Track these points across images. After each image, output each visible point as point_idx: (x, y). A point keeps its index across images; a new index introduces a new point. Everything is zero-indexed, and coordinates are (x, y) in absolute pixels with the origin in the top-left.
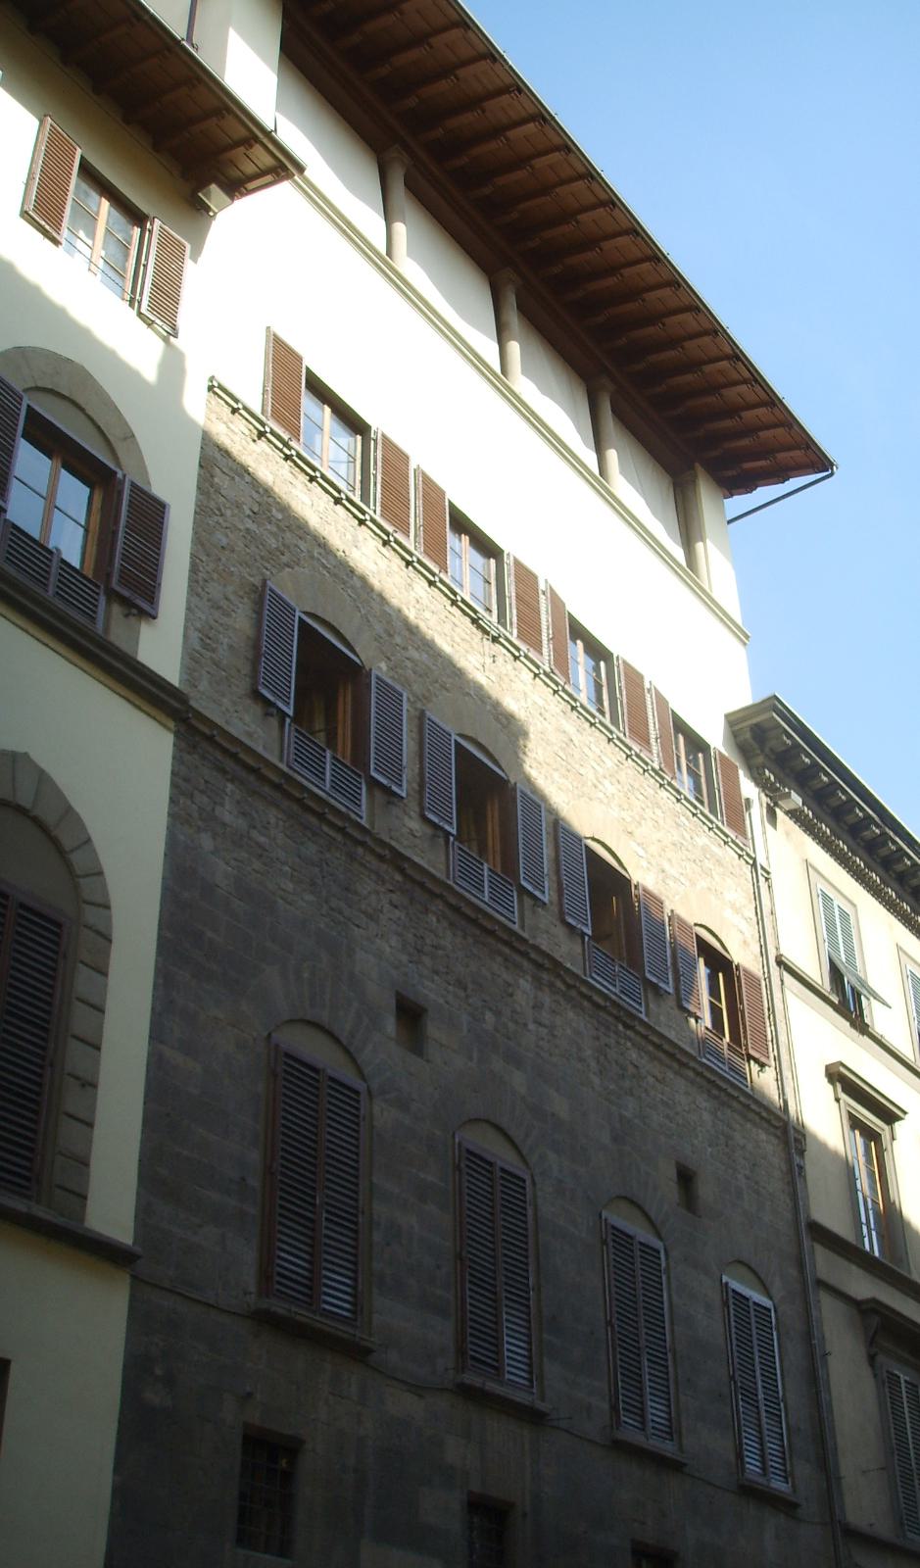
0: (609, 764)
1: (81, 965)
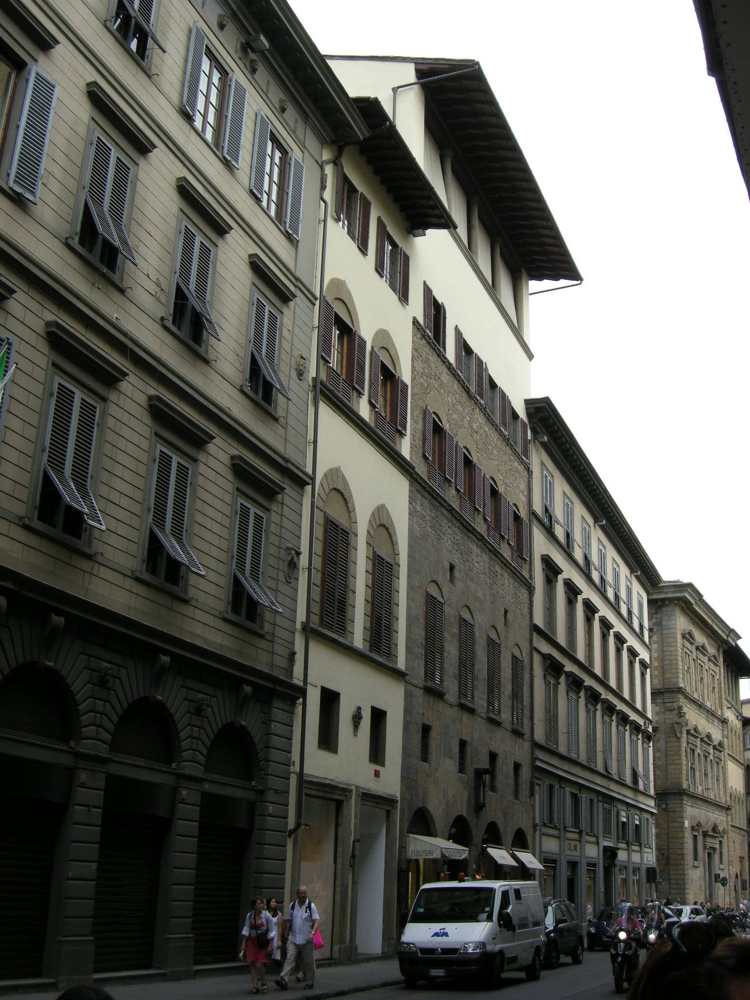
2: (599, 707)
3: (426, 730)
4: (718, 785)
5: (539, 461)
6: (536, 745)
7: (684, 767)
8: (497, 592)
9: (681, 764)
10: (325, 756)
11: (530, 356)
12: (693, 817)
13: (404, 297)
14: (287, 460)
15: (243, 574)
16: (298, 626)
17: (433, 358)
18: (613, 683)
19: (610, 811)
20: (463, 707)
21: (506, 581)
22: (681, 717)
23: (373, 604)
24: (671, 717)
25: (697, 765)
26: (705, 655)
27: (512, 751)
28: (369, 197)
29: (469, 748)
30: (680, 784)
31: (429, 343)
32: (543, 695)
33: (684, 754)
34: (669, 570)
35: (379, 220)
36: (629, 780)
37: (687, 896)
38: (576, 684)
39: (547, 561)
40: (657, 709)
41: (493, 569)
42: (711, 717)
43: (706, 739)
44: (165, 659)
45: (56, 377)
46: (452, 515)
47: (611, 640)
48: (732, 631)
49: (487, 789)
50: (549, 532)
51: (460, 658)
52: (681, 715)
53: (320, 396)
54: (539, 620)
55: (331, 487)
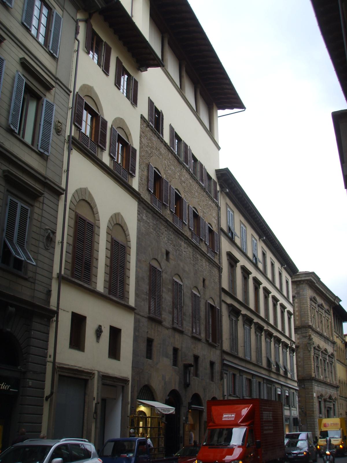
0: (196, 188)
1: (96, 234)
2: (281, 345)
3: (150, 342)
4: (332, 375)
5: (225, 203)
6: (224, 352)
7: (313, 366)
8: (198, 269)
9: (311, 364)
10: (76, 353)
11: (219, 148)
12: (318, 392)
13: (134, 101)
14: (45, 178)
15: (11, 242)
16: (55, 275)
17: (155, 139)
18: (272, 322)
19: (271, 388)
20: (175, 329)
21: (204, 264)
22: (311, 340)
23: (111, 268)
24: (305, 340)
25: (319, 365)
26: (323, 309)
27: (208, 355)
28: (109, 44)
29: (180, 353)
30: (311, 375)
31: (152, 130)
32: (228, 326)
33: (312, 359)
34: (302, 267)
35: (118, 59)
36: (264, 364)
37: (316, 433)
38: (269, 335)
39: (230, 255)
40: (298, 336)
41: (195, 255)
42: (327, 341)
43: (324, 352)
44: (12, 309)
45: (9, 196)
46: (168, 224)
47: (278, 307)
48: (337, 297)
49: (191, 375)
50: (231, 240)
51: (173, 303)
52: (310, 339)
53: (71, 146)
54: (225, 285)
55: (115, 223)
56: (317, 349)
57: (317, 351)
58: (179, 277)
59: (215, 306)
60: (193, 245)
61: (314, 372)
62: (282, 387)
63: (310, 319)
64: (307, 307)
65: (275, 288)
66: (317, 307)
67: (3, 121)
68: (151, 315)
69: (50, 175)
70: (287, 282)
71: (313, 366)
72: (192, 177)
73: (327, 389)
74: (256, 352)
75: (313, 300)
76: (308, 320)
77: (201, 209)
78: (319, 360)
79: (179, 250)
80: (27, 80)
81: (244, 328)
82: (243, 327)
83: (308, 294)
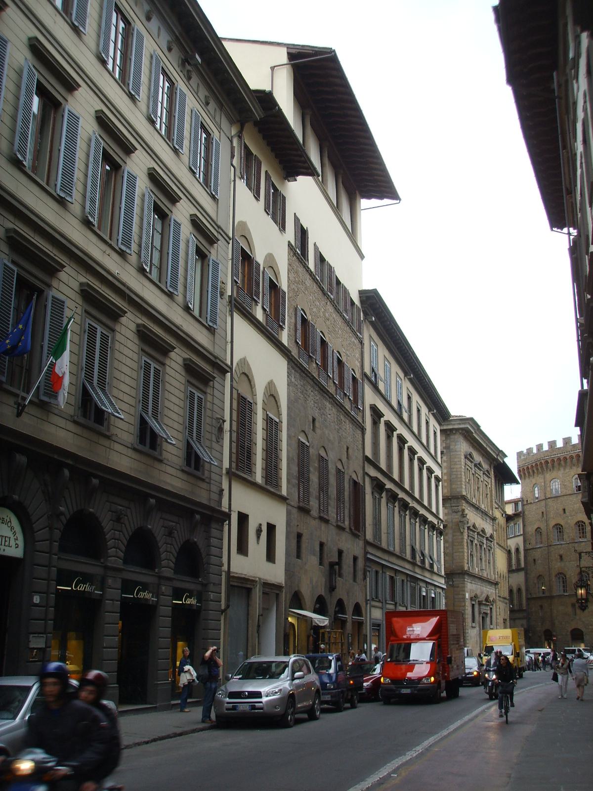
3: (299, 536)
4: (489, 567)
5: (368, 335)
6: (367, 543)
7: (466, 554)
8: (342, 435)
9: (463, 552)
11: (362, 257)
14: (216, 357)
15: (91, 384)
18: (407, 486)
22: (464, 517)
26: (480, 470)
27: (352, 547)
29: (325, 548)
30: (463, 567)
34: (455, 409)
35: (266, 172)
36: (408, 556)
38: (393, 497)
40: (446, 511)
42: (485, 517)
43: (481, 533)
48: (502, 451)
49: (337, 576)
50: (375, 386)
52: (464, 515)
54: (369, 453)
56: (471, 530)
57: (471, 533)
58: (305, 436)
59: (357, 481)
60: (338, 404)
61: (468, 563)
62: (384, 570)
63: (464, 487)
64: (461, 468)
65: (429, 454)
66: (473, 467)
67: (4, 146)
68: (301, 504)
69: (217, 352)
70: (435, 433)
71: (466, 554)
72: (336, 309)
73: (483, 586)
74: (373, 525)
75: (469, 457)
76: (462, 488)
77: (344, 351)
78: (474, 545)
79: (324, 414)
80: (40, 75)
81: (387, 507)
82: (386, 506)
83: (462, 450)
